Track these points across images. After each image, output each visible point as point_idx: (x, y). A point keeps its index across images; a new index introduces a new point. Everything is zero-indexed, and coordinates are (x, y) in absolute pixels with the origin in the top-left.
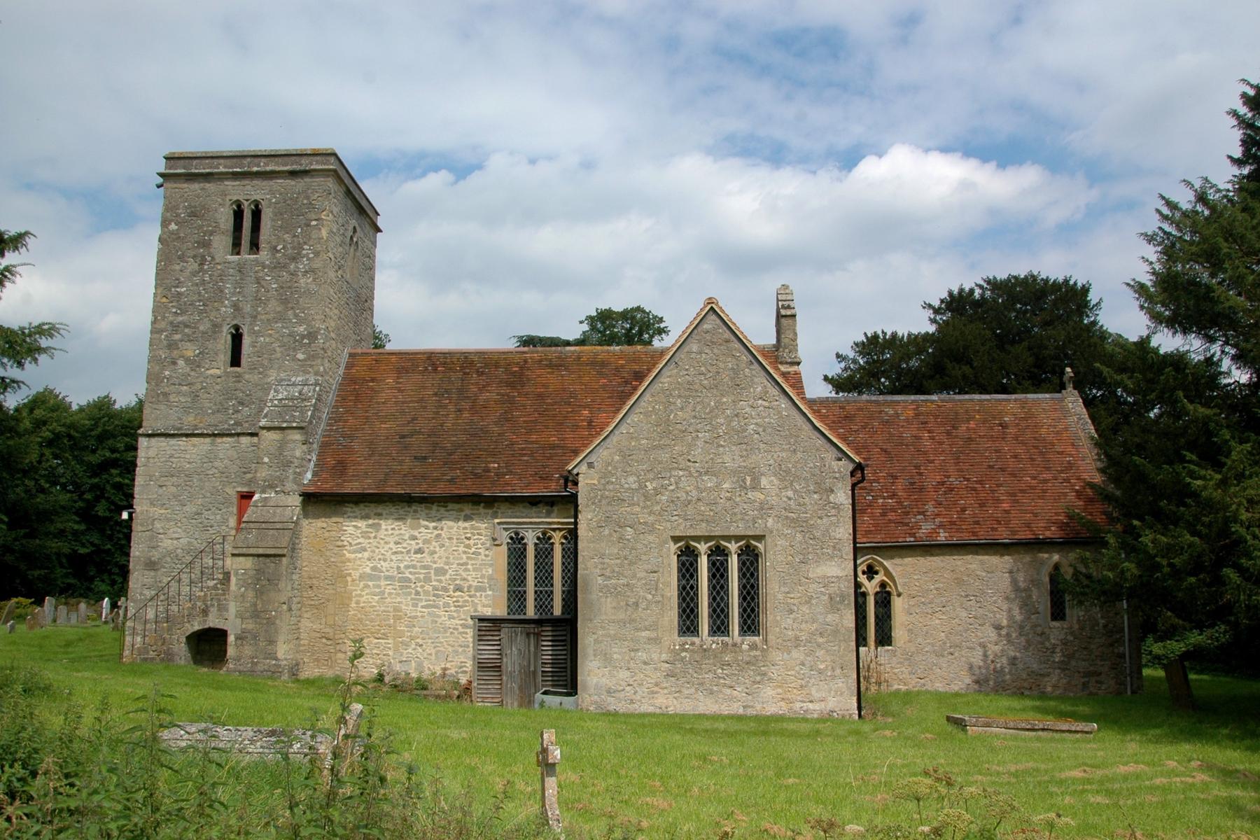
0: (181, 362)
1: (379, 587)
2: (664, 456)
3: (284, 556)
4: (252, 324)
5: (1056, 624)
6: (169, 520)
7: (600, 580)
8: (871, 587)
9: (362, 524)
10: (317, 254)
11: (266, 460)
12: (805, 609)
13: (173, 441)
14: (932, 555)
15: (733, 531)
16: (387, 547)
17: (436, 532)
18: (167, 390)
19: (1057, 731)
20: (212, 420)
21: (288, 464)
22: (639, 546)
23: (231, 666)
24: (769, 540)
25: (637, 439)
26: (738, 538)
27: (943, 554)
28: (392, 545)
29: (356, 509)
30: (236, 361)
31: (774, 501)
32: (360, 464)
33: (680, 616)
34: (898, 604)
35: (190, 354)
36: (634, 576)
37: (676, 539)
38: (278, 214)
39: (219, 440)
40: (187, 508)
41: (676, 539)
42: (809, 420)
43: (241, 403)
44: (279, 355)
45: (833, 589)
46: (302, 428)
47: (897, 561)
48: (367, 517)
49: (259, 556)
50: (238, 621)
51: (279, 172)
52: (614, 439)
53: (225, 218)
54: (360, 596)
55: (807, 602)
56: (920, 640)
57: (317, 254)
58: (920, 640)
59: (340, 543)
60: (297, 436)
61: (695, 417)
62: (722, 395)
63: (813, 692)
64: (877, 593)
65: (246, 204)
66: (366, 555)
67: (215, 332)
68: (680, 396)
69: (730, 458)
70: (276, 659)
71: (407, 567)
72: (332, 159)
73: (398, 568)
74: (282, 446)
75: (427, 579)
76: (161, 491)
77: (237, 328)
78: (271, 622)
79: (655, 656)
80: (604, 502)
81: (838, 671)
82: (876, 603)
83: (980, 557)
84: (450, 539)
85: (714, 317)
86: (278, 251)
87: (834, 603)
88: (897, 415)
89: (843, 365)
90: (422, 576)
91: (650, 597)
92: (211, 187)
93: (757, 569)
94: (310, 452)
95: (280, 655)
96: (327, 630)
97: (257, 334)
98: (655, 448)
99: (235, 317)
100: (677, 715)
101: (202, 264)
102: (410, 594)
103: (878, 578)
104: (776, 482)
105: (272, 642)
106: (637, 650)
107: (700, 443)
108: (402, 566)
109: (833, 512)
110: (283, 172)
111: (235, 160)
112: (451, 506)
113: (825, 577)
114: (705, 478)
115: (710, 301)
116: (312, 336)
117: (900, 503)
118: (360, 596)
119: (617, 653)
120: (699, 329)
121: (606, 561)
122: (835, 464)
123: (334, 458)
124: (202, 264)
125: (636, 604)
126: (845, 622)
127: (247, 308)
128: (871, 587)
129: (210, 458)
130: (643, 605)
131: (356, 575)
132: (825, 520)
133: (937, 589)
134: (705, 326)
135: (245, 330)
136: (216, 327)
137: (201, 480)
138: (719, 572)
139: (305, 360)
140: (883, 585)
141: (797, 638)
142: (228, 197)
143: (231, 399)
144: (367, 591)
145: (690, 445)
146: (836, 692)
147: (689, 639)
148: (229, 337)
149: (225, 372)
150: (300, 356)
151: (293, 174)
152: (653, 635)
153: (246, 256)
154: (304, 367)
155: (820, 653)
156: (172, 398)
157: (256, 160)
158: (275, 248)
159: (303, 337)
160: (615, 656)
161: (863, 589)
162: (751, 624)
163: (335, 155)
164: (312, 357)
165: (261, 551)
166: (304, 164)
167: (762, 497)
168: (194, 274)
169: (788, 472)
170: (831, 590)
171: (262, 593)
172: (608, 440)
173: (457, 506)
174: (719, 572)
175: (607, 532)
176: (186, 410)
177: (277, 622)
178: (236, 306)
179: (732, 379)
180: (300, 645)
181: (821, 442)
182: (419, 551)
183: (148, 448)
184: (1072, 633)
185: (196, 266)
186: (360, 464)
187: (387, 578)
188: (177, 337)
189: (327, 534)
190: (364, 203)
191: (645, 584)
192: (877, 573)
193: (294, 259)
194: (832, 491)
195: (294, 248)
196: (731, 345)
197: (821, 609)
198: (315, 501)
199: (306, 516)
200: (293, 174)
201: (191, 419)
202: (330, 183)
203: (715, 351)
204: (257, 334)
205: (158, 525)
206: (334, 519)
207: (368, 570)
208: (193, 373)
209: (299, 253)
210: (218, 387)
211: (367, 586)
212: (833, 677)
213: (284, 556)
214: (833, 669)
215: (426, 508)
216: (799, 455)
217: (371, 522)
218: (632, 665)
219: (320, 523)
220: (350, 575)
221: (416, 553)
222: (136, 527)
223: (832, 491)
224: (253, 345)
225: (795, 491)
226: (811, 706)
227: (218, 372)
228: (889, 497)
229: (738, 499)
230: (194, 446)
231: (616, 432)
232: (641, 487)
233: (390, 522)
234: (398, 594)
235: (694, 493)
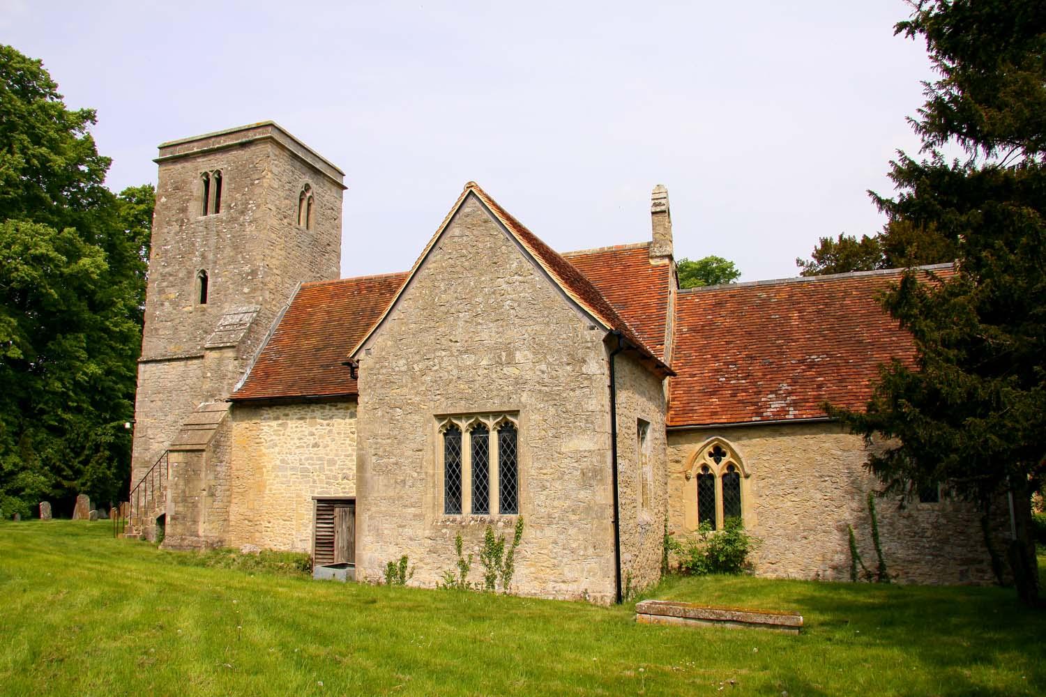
0: (167, 304)
1: (285, 476)
2: (429, 338)
3: (203, 450)
4: (213, 268)
5: (926, 506)
6: (156, 428)
7: (374, 459)
8: (718, 469)
9: (274, 423)
10: (258, 206)
11: (209, 375)
12: (558, 485)
13: (160, 366)
14: (781, 435)
15: (489, 407)
16: (292, 442)
17: (329, 428)
18: (157, 326)
19: (751, 624)
20: (186, 347)
21: (223, 377)
22: (407, 425)
23: (166, 541)
24: (522, 414)
25: (407, 324)
26: (496, 414)
27: (794, 434)
28: (297, 441)
29: (270, 412)
30: (204, 300)
31: (528, 375)
32: (279, 374)
33: (447, 494)
34: (746, 486)
35: (172, 296)
36: (402, 455)
37: (440, 417)
38: (232, 179)
39: (190, 362)
40: (168, 418)
41: (440, 417)
42: (556, 285)
43: (206, 332)
44: (231, 291)
45: (585, 464)
46: (233, 347)
47: (745, 442)
48: (277, 418)
49: (188, 451)
50: (173, 504)
51: (299, 157)
52: (387, 325)
53: (197, 187)
54: (272, 484)
55: (560, 478)
56: (770, 523)
57: (258, 206)
58: (770, 523)
59: (258, 441)
60: (230, 354)
61: (457, 298)
62: (482, 274)
63: (566, 570)
64: (724, 476)
65: (211, 174)
66: (277, 449)
67: (188, 278)
68: (443, 280)
69: (488, 334)
70: (198, 536)
71: (307, 459)
72: (270, 129)
73: (301, 460)
74: (220, 360)
75: (322, 469)
76: (152, 405)
77: (204, 272)
78: (195, 505)
79: (420, 533)
80: (378, 385)
81: (591, 551)
82: (725, 485)
83: (835, 435)
84: (338, 433)
85: (474, 200)
86: (231, 208)
87: (588, 478)
88: (770, 298)
89: (801, 269)
90: (317, 466)
91: (415, 475)
92: (188, 165)
93: (515, 446)
94: (242, 366)
95: (201, 533)
96: (248, 513)
97: (216, 275)
98: (421, 331)
99: (202, 264)
100: (516, 596)
101: (181, 226)
102: (309, 482)
103: (725, 460)
104: (530, 356)
105: (195, 522)
106: (404, 526)
107: (461, 323)
108: (303, 458)
109: (586, 383)
110: (236, 145)
111: (204, 142)
112: (339, 405)
113: (577, 451)
114: (465, 357)
115: (470, 185)
116: (254, 273)
117: (754, 383)
118: (272, 484)
119: (387, 528)
120: (461, 213)
121: (380, 440)
122: (588, 335)
123: (264, 372)
124: (181, 226)
125: (404, 482)
126: (598, 498)
127: (211, 256)
128: (718, 469)
129: (184, 377)
130: (409, 483)
131: (270, 466)
132: (578, 392)
133: (788, 470)
134: (466, 210)
135: (209, 274)
136: (190, 273)
137: (177, 395)
138: (480, 450)
139: (249, 293)
140: (731, 467)
141: (549, 516)
142: (199, 171)
143: (198, 329)
144: (278, 480)
145: (452, 326)
146: (589, 572)
147: (452, 517)
148: (199, 280)
149: (195, 308)
150: (246, 290)
151: (243, 145)
152: (417, 511)
153: (211, 215)
154: (249, 299)
155: (572, 531)
156: (161, 332)
157: (218, 139)
158: (230, 206)
159: (248, 274)
160: (386, 532)
161: (710, 471)
162: (509, 502)
163: (271, 125)
164: (254, 290)
165: (188, 447)
166: (251, 136)
167: (517, 372)
168: (177, 234)
169: (541, 345)
170: (584, 465)
171: (189, 482)
172: (383, 327)
173: (344, 405)
174: (480, 450)
175: (380, 414)
176: (170, 341)
177: (199, 505)
178: (203, 257)
179: (489, 258)
180: (229, 526)
181: (575, 311)
182: (316, 445)
183: (145, 372)
184: (945, 516)
185: (177, 228)
186: (279, 374)
187: (292, 469)
188: (165, 284)
189: (249, 433)
190: (318, 166)
191: (412, 462)
192: (724, 454)
193: (242, 213)
194: (584, 361)
195: (242, 204)
196: (489, 225)
197: (572, 485)
198: (244, 405)
199: (234, 419)
200: (243, 145)
201: (172, 347)
202: (269, 148)
203: (475, 232)
204: (216, 275)
205: (150, 432)
206: (254, 421)
207: (278, 463)
208: (174, 311)
209: (246, 208)
210: (190, 321)
211: (277, 476)
212: (586, 557)
213: (203, 450)
214: (586, 549)
215: (322, 408)
216: (552, 327)
217: (280, 422)
218: (400, 540)
219: (244, 424)
220: (265, 466)
221: (313, 447)
222: (137, 434)
223: (584, 361)
224: (214, 284)
225: (549, 364)
226: (563, 586)
227: (191, 309)
228: (743, 378)
229: (494, 376)
230: (173, 368)
231: (390, 319)
232: (409, 370)
233: (294, 421)
234: (300, 483)
235: (455, 372)
